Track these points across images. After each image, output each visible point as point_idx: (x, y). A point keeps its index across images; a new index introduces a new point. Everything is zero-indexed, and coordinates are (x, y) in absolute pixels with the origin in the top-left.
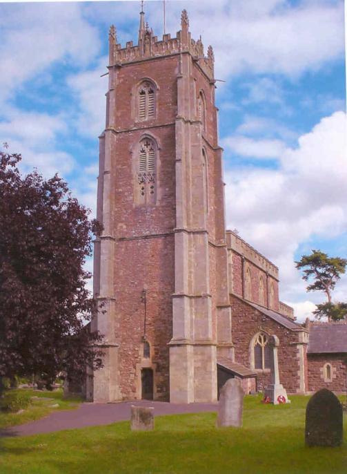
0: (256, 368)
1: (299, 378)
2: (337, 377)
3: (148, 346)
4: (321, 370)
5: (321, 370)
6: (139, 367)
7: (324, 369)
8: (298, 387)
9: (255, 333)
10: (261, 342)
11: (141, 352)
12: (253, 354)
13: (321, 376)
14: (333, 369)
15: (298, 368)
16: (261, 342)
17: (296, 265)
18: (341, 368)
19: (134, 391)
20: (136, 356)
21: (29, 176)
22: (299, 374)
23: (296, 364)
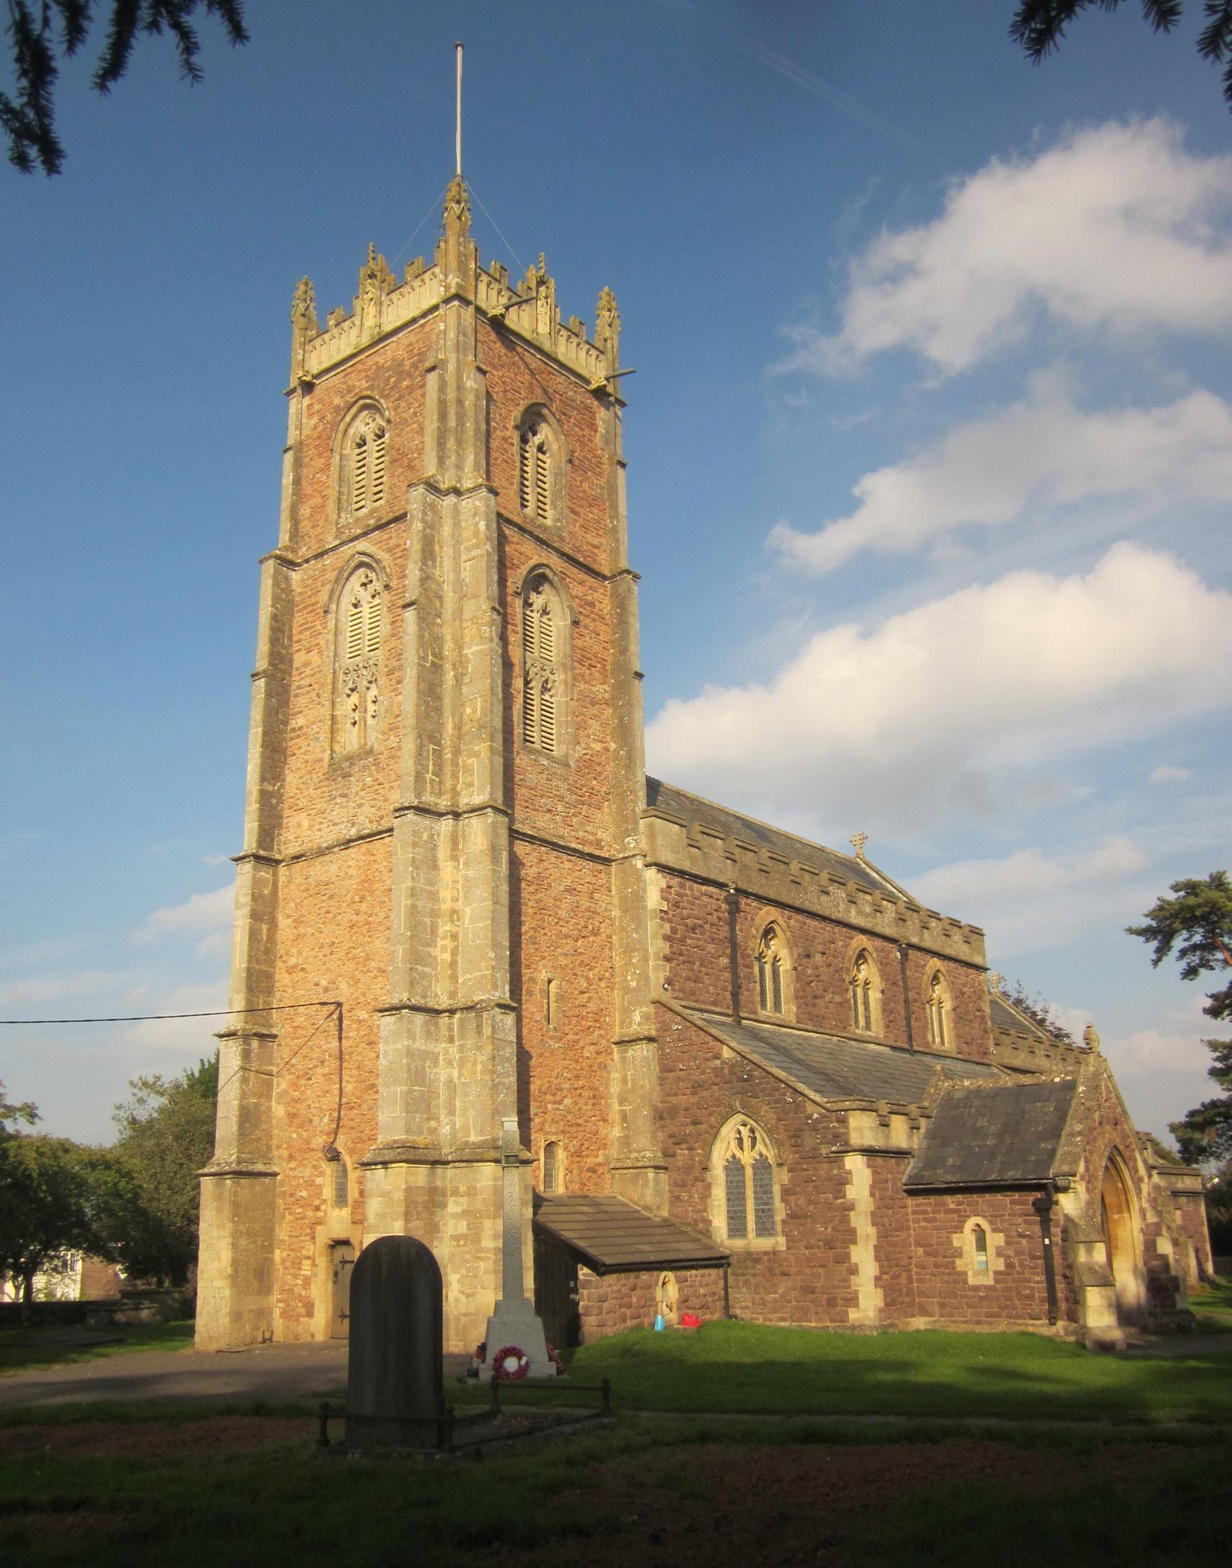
0: (758, 1235)
1: (854, 1271)
2: (1009, 1265)
3: (345, 1171)
4: (956, 1240)
5: (956, 1240)
6: (324, 1235)
7: (965, 1239)
8: (853, 1301)
9: (725, 1119)
10: (741, 1147)
11: (328, 1192)
12: (719, 1193)
13: (958, 1262)
14: (995, 1240)
15: (851, 1237)
16: (741, 1147)
17: (97, 91)
18: (1021, 1236)
19: (310, 1314)
20: (317, 1202)
21: (772, 922)
22: (855, 1259)
23: (845, 1220)
